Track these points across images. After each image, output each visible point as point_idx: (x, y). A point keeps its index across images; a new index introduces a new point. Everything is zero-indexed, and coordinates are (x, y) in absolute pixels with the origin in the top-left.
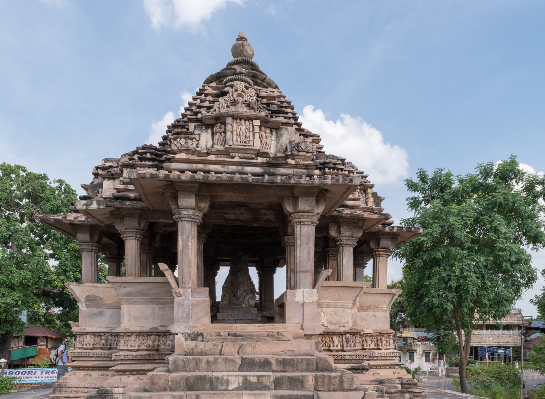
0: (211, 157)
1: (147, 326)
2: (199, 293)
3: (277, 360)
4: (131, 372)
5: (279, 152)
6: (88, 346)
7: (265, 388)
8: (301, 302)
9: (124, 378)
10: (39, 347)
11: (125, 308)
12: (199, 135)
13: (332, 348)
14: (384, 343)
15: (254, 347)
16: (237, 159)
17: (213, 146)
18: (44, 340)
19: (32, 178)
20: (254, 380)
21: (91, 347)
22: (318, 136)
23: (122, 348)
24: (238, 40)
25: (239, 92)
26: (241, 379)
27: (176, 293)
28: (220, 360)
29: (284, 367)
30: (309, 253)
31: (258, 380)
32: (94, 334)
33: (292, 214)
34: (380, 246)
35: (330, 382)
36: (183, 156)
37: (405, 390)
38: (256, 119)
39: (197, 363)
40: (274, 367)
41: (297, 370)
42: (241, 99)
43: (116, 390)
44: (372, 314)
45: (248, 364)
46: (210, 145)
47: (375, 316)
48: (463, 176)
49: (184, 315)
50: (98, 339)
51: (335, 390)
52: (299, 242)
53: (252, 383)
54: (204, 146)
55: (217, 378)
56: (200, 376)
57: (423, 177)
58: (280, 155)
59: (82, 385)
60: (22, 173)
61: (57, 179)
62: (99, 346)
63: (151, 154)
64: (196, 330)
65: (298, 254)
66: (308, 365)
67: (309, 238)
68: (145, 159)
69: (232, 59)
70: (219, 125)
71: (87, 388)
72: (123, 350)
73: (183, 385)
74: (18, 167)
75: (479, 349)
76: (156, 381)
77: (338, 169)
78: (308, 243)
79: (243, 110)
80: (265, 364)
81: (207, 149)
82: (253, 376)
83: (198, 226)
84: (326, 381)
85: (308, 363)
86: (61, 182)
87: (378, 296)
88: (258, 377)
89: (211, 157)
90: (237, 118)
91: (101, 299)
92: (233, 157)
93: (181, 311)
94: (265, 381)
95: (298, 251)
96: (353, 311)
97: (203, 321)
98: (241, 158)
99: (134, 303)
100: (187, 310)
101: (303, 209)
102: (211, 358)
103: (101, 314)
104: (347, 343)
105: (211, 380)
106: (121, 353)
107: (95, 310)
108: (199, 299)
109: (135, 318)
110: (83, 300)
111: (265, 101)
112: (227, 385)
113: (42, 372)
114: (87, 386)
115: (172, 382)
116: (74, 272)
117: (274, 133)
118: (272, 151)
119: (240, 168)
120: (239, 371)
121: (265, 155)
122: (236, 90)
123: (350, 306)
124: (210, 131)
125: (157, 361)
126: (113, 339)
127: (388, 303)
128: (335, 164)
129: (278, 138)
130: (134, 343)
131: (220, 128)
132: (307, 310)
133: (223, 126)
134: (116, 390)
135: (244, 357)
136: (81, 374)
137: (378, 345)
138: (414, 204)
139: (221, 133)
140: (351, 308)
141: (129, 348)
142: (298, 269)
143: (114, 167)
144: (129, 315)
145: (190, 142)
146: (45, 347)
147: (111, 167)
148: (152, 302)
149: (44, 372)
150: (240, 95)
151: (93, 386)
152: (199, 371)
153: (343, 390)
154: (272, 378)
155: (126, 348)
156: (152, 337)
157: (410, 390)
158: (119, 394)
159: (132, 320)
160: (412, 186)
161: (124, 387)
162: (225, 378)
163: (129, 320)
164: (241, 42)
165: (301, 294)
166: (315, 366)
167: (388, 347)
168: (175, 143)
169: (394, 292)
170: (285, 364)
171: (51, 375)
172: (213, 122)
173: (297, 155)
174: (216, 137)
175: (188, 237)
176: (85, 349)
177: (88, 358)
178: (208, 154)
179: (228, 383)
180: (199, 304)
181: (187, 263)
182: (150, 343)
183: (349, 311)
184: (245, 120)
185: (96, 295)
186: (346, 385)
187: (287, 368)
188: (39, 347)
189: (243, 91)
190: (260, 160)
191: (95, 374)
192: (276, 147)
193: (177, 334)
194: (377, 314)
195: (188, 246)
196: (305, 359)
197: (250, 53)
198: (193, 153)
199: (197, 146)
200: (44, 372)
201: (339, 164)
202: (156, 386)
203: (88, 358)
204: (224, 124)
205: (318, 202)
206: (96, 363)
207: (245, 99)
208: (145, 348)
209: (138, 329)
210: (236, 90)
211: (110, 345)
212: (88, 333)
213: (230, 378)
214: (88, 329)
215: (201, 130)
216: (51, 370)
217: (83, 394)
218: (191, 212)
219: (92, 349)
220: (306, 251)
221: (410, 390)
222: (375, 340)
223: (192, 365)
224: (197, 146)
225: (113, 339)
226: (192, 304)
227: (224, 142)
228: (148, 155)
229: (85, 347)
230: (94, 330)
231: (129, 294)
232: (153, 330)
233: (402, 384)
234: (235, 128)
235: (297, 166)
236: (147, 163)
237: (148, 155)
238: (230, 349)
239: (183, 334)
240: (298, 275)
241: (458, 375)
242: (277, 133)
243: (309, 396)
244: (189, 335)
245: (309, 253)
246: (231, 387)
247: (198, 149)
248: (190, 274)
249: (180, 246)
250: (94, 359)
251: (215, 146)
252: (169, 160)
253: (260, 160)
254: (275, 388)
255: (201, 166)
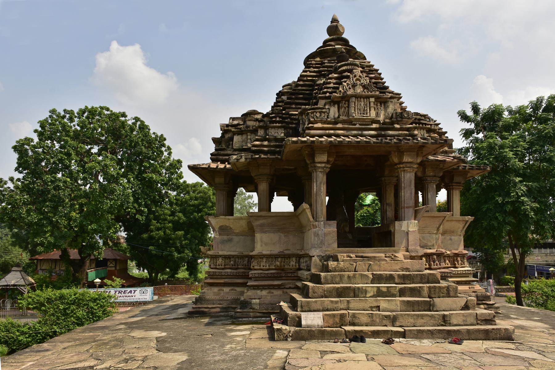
0: (340, 125)
1: (276, 250)
2: (329, 225)
3: (399, 275)
4: (262, 287)
5: (387, 119)
6: (220, 267)
7: (394, 296)
8: (406, 230)
9: (259, 292)
10: (109, 269)
11: (258, 236)
12: (329, 109)
13: (433, 267)
14: (460, 262)
15: (380, 265)
16: (358, 126)
17: (339, 117)
18: (114, 263)
19: (115, 117)
20: (385, 290)
21: (223, 267)
22: (400, 94)
23: (256, 267)
24: (332, 22)
25: (357, 77)
26: (375, 289)
27: (313, 225)
28: (357, 276)
29: (404, 280)
30: (411, 193)
31: (388, 290)
32: (225, 257)
33: (396, 164)
34: (454, 181)
35: (440, 291)
36: (319, 125)
37: (480, 302)
38: (372, 97)
39: (341, 277)
40: (397, 280)
41: (413, 283)
42: (358, 82)
43: (254, 301)
44: (448, 238)
45: (377, 279)
46: (337, 115)
47: (451, 239)
48: (514, 107)
49: (319, 242)
50: (227, 261)
51: (443, 297)
52: (403, 185)
53: (383, 292)
54: (332, 117)
55: (358, 288)
56: (347, 287)
57: (476, 109)
58: (387, 120)
59: (217, 297)
60: (106, 112)
61: (133, 117)
62: (229, 266)
63: (280, 118)
64: (328, 253)
65: (403, 194)
66: (421, 278)
67: (411, 182)
68: (276, 122)
69: (327, 37)
70: (344, 102)
71: (221, 300)
72: (256, 270)
73: (334, 293)
74: (102, 108)
75: (528, 267)
76: (316, 290)
77: (423, 124)
78: (410, 186)
79: (359, 90)
80: (390, 279)
81: (334, 118)
82: (384, 287)
83: (327, 174)
84: (437, 290)
85: (422, 277)
86: (137, 119)
87: (453, 223)
88: (388, 287)
89: (340, 125)
90: (358, 97)
91: (231, 228)
92: (355, 125)
93: (316, 238)
94: (393, 291)
95: (403, 191)
96: (437, 236)
97: (332, 246)
98: (360, 125)
99: (265, 232)
100: (321, 238)
101: (406, 161)
102: (351, 274)
103: (230, 240)
104: (434, 263)
105: (354, 290)
106: (256, 272)
107: (225, 237)
108: (329, 230)
109: (266, 244)
110: (217, 230)
111: (374, 81)
112: (366, 294)
113: (116, 292)
114: (221, 298)
115: (327, 291)
116: (145, 199)
117: (383, 105)
118: (381, 118)
119: (360, 132)
120: (371, 283)
121: (377, 122)
122: (355, 76)
123: (435, 232)
124: (336, 106)
125: (283, 278)
126: (239, 261)
127: (461, 228)
128: (420, 120)
129: (386, 108)
130: (264, 264)
131: (345, 104)
132: (411, 238)
133: (347, 103)
134: (254, 301)
135: (375, 273)
136: (216, 289)
137: (455, 264)
138: (467, 134)
139: (345, 108)
140: (436, 234)
141: (262, 267)
142: (403, 205)
143: (241, 125)
144: (262, 241)
145: (323, 115)
146: (114, 269)
147: (238, 124)
148: (279, 231)
149: (118, 292)
150: (357, 80)
151: (226, 299)
152: (343, 284)
153: (449, 297)
154: (398, 289)
155: (259, 268)
156: (279, 259)
157: (484, 302)
158: (256, 304)
159: (264, 245)
160: (464, 117)
161: (259, 299)
162: (364, 288)
163: (261, 246)
164: (335, 24)
165: (406, 225)
166: (426, 280)
167: (463, 266)
168: (312, 115)
169: (467, 219)
170: (405, 279)
171: (123, 295)
172: (340, 99)
173: (401, 121)
174: (342, 110)
175: (321, 183)
176: (218, 269)
177: (221, 276)
178: (336, 123)
179: (366, 292)
180: (329, 233)
181: (320, 203)
182: (278, 263)
183: (434, 236)
184: (364, 98)
185: (227, 225)
186: (452, 294)
187: (406, 282)
188: (109, 269)
189: (360, 76)
190: (374, 126)
191: (226, 289)
192: (385, 115)
193: (314, 256)
194: (453, 237)
195: (321, 189)
196: (419, 274)
197: (342, 31)
198: (325, 123)
199: (328, 118)
200: (118, 292)
201: (422, 120)
202: (316, 294)
203: (221, 276)
204: (349, 101)
205: (418, 155)
206: (226, 280)
207: (362, 82)
208: (274, 267)
209: (268, 253)
210: (355, 76)
211: (238, 265)
212: (220, 256)
213: (367, 289)
214: (221, 253)
215: (330, 106)
216: (123, 290)
217: (219, 306)
218: (323, 165)
219: (223, 269)
220: (409, 192)
221: (484, 302)
222: (452, 260)
223: (338, 279)
224: (328, 118)
225: (239, 261)
226: (325, 234)
227: (348, 114)
228: (278, 119)
229: (218, 267)
230: (225, 253)
231: (261, 225)
232: (281, 254)
233: (477, 296)
234: (356, 104)
235: (401, 129)
236: (277, 125)
237: (278, 119)
238: (362, 265)
239: (318, 256)
240: (403, 210)
241: (514, 294)
242: (385, 105)
243: (427, 301)
244: (323, 257)
245: (411, 193)
246: (368, 295)
247: (329, 119)
248: (322, 210)
249: (315, 190)
250: (219, 277)
251: (341, 117)
252: (309, 129)
253: (374, 126)
254: (400, 296)
255: (332, 132)
